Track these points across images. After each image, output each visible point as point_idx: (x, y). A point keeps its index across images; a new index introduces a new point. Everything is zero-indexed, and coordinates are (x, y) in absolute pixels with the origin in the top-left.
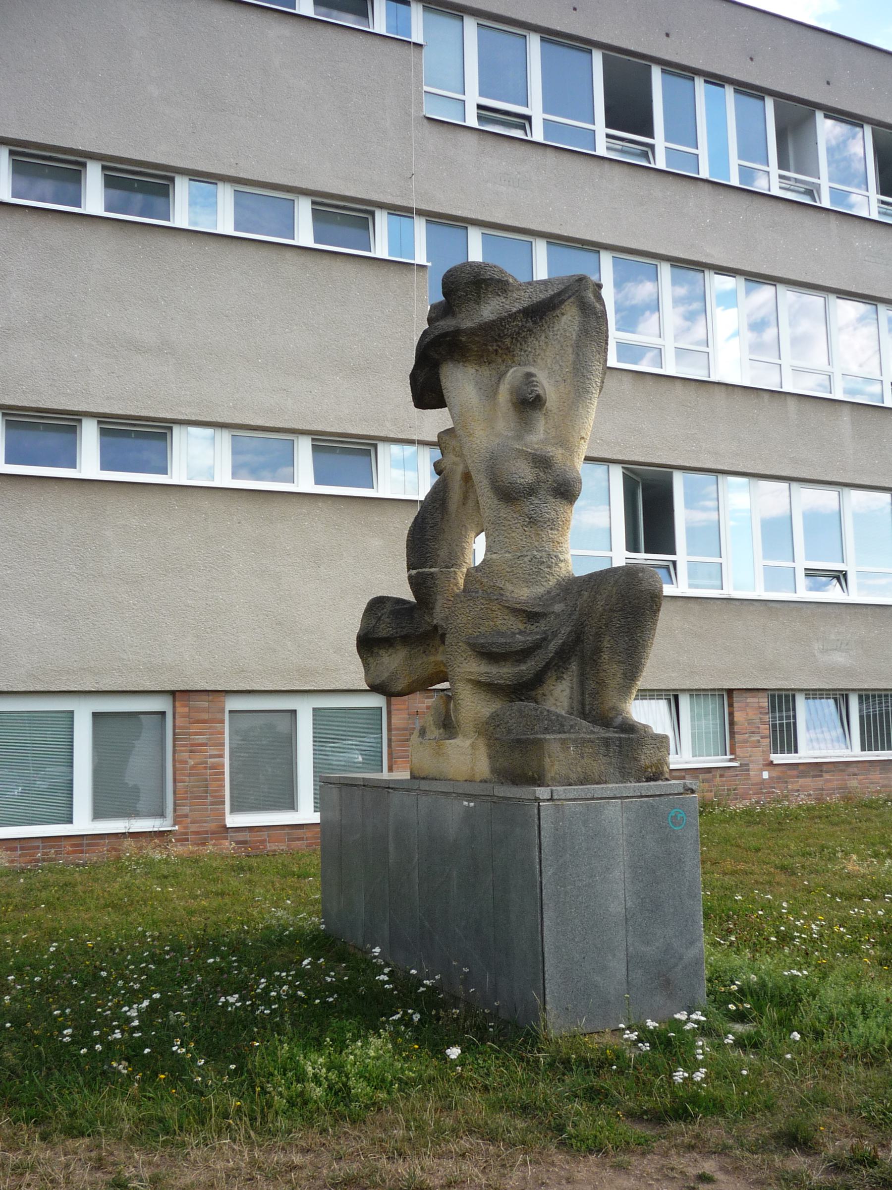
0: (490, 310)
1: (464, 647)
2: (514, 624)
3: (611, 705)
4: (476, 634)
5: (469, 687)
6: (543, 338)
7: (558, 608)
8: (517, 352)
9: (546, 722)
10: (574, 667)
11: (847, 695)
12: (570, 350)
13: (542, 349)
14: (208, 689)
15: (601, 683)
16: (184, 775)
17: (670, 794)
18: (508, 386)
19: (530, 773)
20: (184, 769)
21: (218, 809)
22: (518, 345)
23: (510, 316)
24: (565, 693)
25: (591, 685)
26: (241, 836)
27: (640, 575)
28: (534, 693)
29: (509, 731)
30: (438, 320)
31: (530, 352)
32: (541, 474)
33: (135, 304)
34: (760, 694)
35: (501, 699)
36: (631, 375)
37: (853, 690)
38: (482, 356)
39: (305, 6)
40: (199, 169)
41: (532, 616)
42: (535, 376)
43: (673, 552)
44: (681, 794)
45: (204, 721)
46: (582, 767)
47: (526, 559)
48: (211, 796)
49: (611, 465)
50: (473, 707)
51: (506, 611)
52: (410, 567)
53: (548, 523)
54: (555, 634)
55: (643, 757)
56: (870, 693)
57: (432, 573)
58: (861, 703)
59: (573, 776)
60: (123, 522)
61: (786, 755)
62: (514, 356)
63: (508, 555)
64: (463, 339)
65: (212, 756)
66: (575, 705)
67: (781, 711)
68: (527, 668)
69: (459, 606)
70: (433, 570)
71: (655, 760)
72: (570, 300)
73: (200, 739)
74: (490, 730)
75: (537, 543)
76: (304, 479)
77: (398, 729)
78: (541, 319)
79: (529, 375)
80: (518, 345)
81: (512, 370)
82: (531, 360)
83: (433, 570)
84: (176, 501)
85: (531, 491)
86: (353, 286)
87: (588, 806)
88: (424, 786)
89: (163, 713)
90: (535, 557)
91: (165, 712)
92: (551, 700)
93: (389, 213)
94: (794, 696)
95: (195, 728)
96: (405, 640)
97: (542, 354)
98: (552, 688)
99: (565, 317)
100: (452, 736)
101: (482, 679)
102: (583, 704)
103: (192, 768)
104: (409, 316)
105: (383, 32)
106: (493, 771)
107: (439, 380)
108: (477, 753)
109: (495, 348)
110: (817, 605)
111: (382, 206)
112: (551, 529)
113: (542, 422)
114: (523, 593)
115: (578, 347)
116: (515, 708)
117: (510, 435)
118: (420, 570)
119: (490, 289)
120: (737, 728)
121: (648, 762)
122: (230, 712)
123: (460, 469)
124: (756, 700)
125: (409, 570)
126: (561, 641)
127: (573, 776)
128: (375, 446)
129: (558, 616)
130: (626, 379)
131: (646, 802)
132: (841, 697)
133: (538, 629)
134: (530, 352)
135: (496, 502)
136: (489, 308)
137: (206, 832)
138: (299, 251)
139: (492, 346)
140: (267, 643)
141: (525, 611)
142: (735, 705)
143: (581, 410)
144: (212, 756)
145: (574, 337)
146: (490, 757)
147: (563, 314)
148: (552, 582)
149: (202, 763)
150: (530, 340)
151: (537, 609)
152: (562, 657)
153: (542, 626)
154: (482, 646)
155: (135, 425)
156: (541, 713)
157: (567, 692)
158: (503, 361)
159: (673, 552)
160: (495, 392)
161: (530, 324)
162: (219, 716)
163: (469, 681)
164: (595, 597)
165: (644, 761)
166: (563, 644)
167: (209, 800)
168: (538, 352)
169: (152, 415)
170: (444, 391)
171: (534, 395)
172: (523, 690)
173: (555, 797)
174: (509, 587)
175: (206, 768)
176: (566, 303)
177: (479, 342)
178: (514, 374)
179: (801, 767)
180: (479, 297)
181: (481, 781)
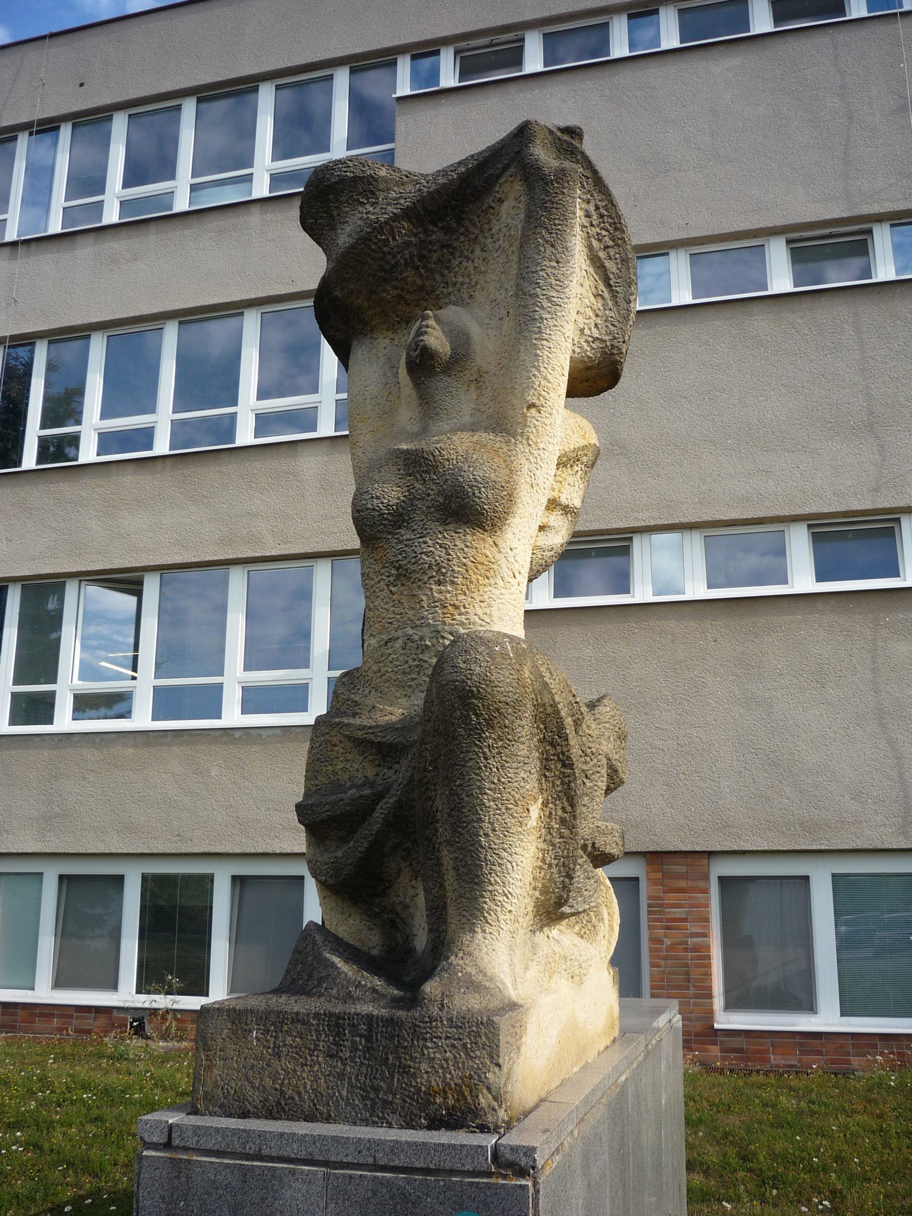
6: (478, 252)
13: (481, 273)
14: (683, 849)
17: (452, 1172)
21: (702, 1004)
22: (438, 278)
26: (734, 1042)
32: (418, 485)
33: (579, 407)
39: (762, 20)
40: (644, 242)
44: (489, 1175)
45: (682, 890)
46: (274, 1077)
47: (399, 644)
48: (694, 986)
55: (424, 1066)
59: (255, 1097)
60: (576, 654)
65: (693, 935)
71: (454, 1075)
72: (508, 173)
73: (678, 913)
75: (410, 613)
76: (802, 579)
78: (460, 221)
80: (438, 278)
82: (466, 296)
84: (636, 622)
86: (845, 326)
87: (245, 1172)
90: (409, 638)
91: (637, 879)
93: (892, 225)
103: (670, 948)
105: (865, 14)
111: (879, 218)
112: (439, 583)
119: (344, 199)
121: (436, 1082)
122: (721, 879)
127: (255, 1097)
131: (388, 1184)
138: (770, 302)
139: (384, 291)
140: (757, 790)
141: (371, 743)
143: (522, 356)
144: (693, 935)
147: (501, 201)
149: (680, 944)
161: (437, 235)
162: (701, 884)
165: (427, 1076)
167: (692, 991)
169: (603, 526)
173: (176, 1142)
175: (686, 950)
180: (331, 217)
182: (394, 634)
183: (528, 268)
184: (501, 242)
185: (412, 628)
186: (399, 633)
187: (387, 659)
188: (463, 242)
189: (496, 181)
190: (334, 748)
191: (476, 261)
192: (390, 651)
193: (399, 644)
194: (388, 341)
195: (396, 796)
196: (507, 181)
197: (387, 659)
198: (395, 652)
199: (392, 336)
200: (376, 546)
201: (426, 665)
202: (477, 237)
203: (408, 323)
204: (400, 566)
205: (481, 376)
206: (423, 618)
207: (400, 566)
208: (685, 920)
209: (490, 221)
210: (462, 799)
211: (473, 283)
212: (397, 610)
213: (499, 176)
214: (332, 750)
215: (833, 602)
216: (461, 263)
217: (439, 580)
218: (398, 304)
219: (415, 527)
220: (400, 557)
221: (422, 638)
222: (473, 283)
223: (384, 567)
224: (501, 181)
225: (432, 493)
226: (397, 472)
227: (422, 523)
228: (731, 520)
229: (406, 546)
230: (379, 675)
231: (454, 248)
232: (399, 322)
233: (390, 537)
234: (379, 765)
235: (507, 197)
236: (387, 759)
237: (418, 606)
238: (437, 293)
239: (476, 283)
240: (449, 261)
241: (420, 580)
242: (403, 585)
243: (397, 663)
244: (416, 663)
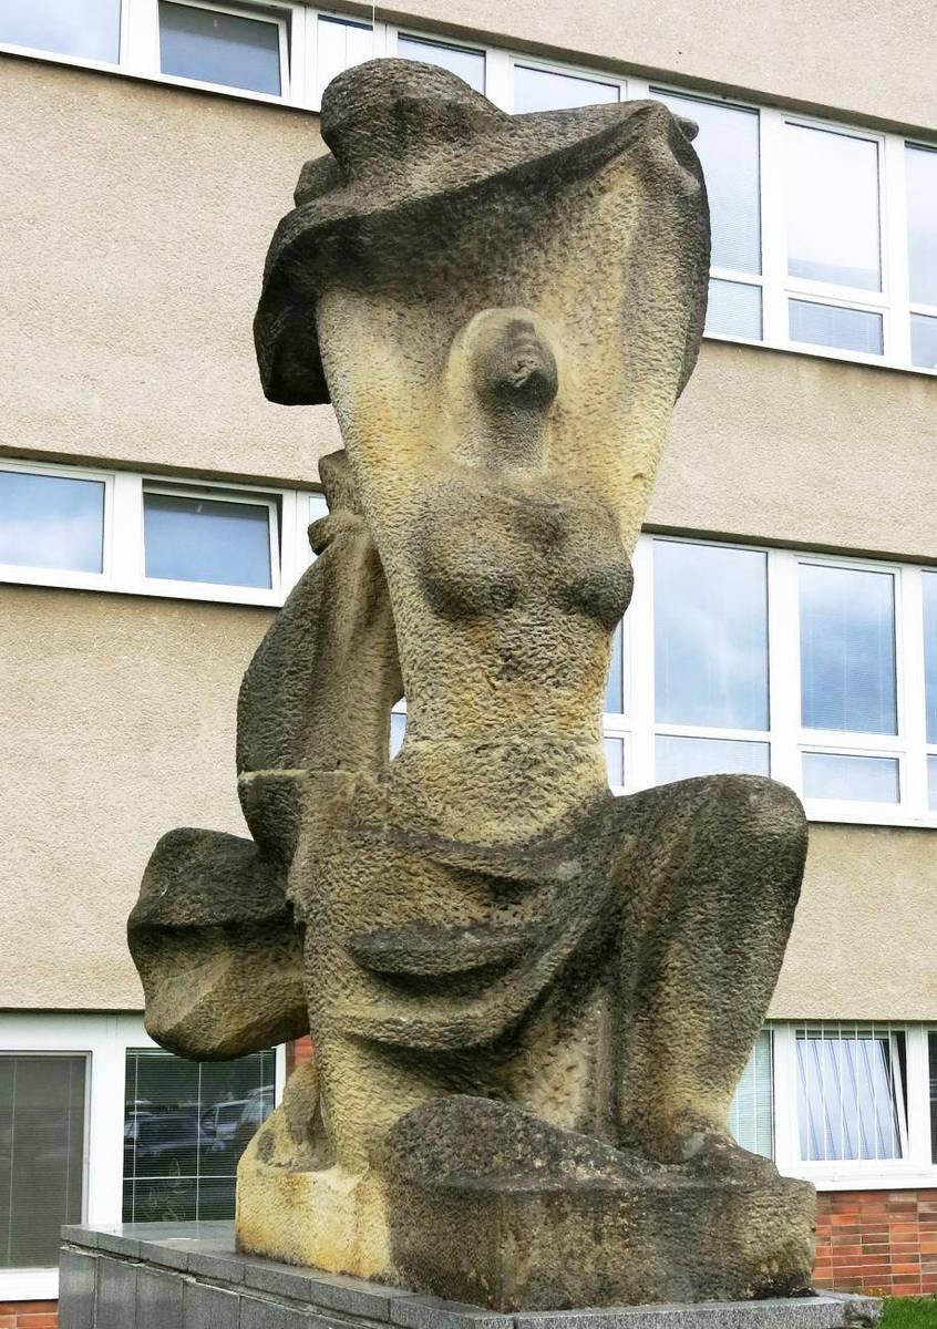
0: (425, 174)
1: (343, 958)
2: (458, 907)
3: (680, 1105)
4: (370, 929)
5: (352, 1052)
6: (556, 243)
7: (566, 869)
8: (495, 273)
9: (519, 1147)
10: (597, 1010)
12: (617, 273)
15: (659, 1054)
18: (470, 353)
19: (473, 1274)
22: (499, 260)
23: (474, 188)
24: (577, 1074)
25: (637, 1059)
27: (753, 798)
28: (502, 1073)
29: (435, 1166)
30: (315, 196)
31: (525, 276)
35: (427, 1085)
36: (817, 367)
38: (412, 282)
41: (504, 891)
42: (531, 328)
47: (497, 754)
49: (771, 552)
51: (443, 877)
52: (243, 764)
53: (551, 672)
54: (554, 933)
57: (290, 781)
62: (487, 283)
63: (453, 743)
64: (366, 240)
66: (599, 1101)
68: (484, 1014)
69: (336, 860)
70: (289, 773)
72: (620, 159)
74: (401, 1162)
75: (521, 718)
79: (517, 327)
80: (499, 260)
81: (480, 316)
82: (527, 293)
83: (289, 773)
85: (509, 596)
90: (516, 748)
92: (545, 1089)
96: (233, 932)
97: (553, 282)
98: (548, 1059)
99: (608, 197)
100: (323, 1165)
101: (381, 1035)
102: (616, 1101)
104: (249, 190)
106: (399, 1257)
107: (315, 336)
108: (367, 1209)
109: (442, 262)
110: (869, 1197)
112: (557, 684)
113: (548, 436)
116: (451, 1109)
117: (470, 464)
118: (264, 773)
123: (362, 542)
125: (239, 771)
126: (566, 951)
128: (278, 500)
129: (563, 888)
130: (809, 373)
133: (516, 921)
134: (525, 276)
135: (430, 618)
136: (427, 169)
139: (433, 258)
141: (486, 877)
145: (627, 243)
147: (603, 190)
148: (559, 809)
150: (524, 247)
151: (515, 873)
152: (573, 983)
153: (515, 918)
154: (382, 957)
155: (208, 490)
156: (511, 1123)
157: (581, 1072)
158: (462, 294)
160: (441, 366)
164: (648, 846)
166: (573, 957)
168: (544, 275)
170: (325, 361)
171: (525, 373)
172: (473, 1068)
174: (453, 816)
176: (610, 166)
177: (402, 248)
178: (483, 327)
181: (372, 1279)
182: (493, 740)
183: (652, 301)
184: (590, 242)
185: (521, 736)
186: (502, 740)
187: (476, 769)
188: (543, 226)
189: (604, 164)
190: (414, 878)
191: (550, 254)
192: (484, 760)
193: (501, 751)
194: (394, 316)
195: (569, 946)
196: (615, 169)
197: (476, 769)
198: (491, 763)
199: (402, 311)
200: (473, 622)
201: (532, 784)
202: (561, 224)
203: (430, 300)
204: (511, 657)
205: (560, 415)
206: (536, 726)
207: (511, 657)
209: (582, 209)
210: (749, 958)
211: (541, 280)
212: (500, 711)
213: (608, 159)
214: (410, 880)
215: (176, 614)
216: (531, 249)
217: (558, 682)
218: (436, 276)
219: (534, 610)
220: (513, 645)
221: (531, 750)
222: (541, 280)
223: (484, 653)
224: (610, 166)
225: (556, 570)
226: (504, 532)
227: (543, 607)
228: (25, 450)
229: (522, 632)
230: (460, 788)
231: (532, 230)
232: (420, 297)
233: (496, 615)
234: (488, 905)
235: (611, 190)
236: (501, 897)
237: (531, 710)
238: (490, 277)
239: (545, 282)
240: (519, 243)
241: (536, 678)
242: (509, 680)
243: (493, 777)
244: (520, 780)
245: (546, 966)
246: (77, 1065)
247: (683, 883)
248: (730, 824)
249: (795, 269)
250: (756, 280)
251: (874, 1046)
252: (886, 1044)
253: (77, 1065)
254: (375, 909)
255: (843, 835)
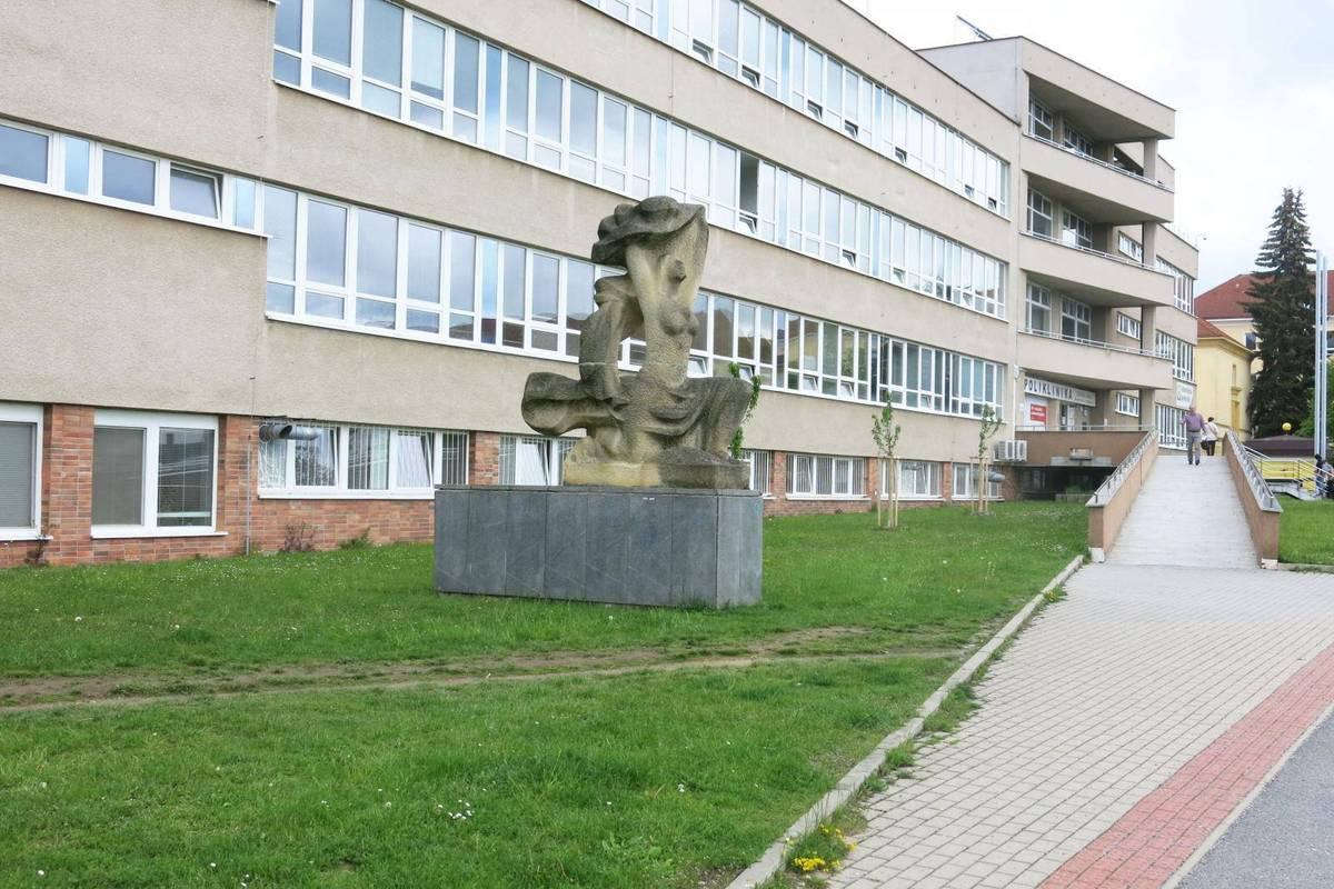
1: (647, 413)
2: (671, 403)
7: (692, 396)
11: (433, 434)
16: (56, 486)
20: (58, 481)
25: (710, 439)
34: (495, 437)
36: (423, 135)
37: (345, 423)
43: (568, 335)
45: (76, 435)
50: (646, 446)
56: (448, 433)
58: (444, 445)
61: (360, 491)
67: (450, 446)
73: (72, 452)
77: (231, 452)
88: (571, 488)
89: (33, 425)
94: (338, 429)
95: (69, 441)
103: (64, 480)
106: (664, 481)
114: (674, 385)
115: (697, 246)
120: (477, 466)
124: (491, 442)
132: (427, 435)
137: (74, 543)
142: (477, 445)
146: (661, 474)
159: (568, 335)
163: (647, 432)
178: (668, 262)
179: (372, 507)
208: (75, 458)
245: (694, 417)
246: (141, 433)
247: (726, 401)
248: (739, 389)
249: (416, 87)
250: (398, 89)
251: (416, 440)
252: (423, 439)
253: (141, 433)
254: (655, 402)
255: (422, 347)
